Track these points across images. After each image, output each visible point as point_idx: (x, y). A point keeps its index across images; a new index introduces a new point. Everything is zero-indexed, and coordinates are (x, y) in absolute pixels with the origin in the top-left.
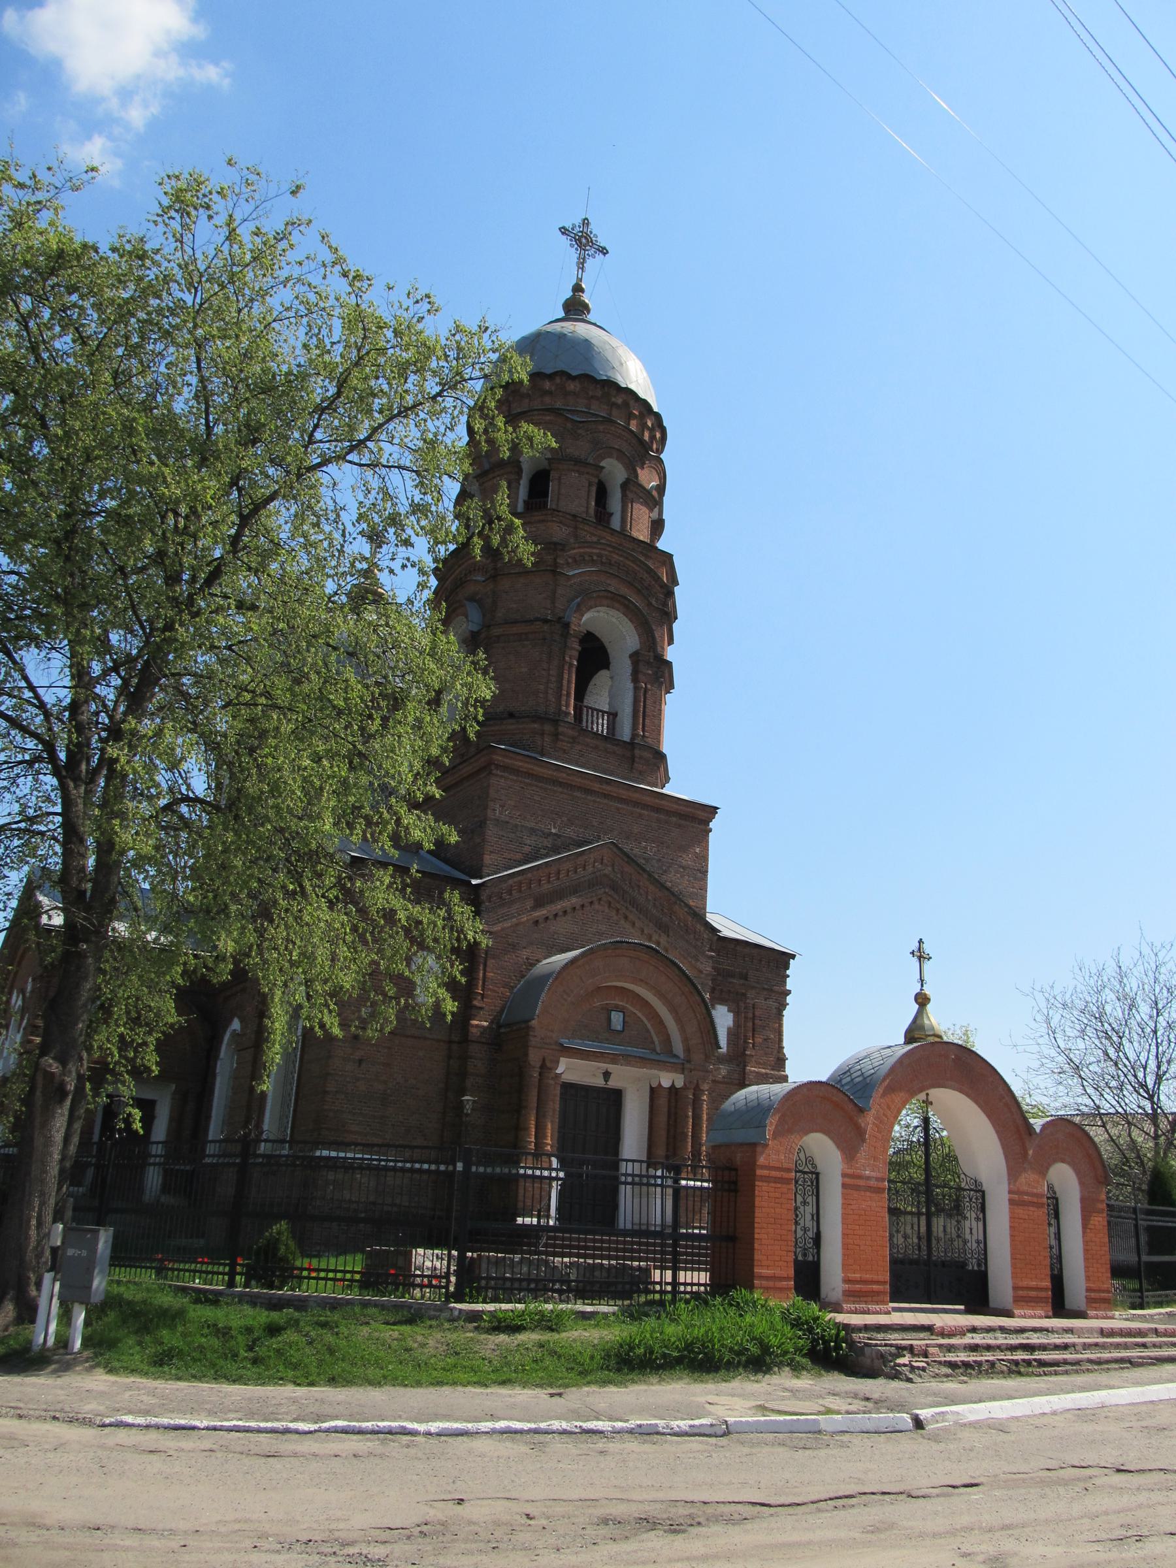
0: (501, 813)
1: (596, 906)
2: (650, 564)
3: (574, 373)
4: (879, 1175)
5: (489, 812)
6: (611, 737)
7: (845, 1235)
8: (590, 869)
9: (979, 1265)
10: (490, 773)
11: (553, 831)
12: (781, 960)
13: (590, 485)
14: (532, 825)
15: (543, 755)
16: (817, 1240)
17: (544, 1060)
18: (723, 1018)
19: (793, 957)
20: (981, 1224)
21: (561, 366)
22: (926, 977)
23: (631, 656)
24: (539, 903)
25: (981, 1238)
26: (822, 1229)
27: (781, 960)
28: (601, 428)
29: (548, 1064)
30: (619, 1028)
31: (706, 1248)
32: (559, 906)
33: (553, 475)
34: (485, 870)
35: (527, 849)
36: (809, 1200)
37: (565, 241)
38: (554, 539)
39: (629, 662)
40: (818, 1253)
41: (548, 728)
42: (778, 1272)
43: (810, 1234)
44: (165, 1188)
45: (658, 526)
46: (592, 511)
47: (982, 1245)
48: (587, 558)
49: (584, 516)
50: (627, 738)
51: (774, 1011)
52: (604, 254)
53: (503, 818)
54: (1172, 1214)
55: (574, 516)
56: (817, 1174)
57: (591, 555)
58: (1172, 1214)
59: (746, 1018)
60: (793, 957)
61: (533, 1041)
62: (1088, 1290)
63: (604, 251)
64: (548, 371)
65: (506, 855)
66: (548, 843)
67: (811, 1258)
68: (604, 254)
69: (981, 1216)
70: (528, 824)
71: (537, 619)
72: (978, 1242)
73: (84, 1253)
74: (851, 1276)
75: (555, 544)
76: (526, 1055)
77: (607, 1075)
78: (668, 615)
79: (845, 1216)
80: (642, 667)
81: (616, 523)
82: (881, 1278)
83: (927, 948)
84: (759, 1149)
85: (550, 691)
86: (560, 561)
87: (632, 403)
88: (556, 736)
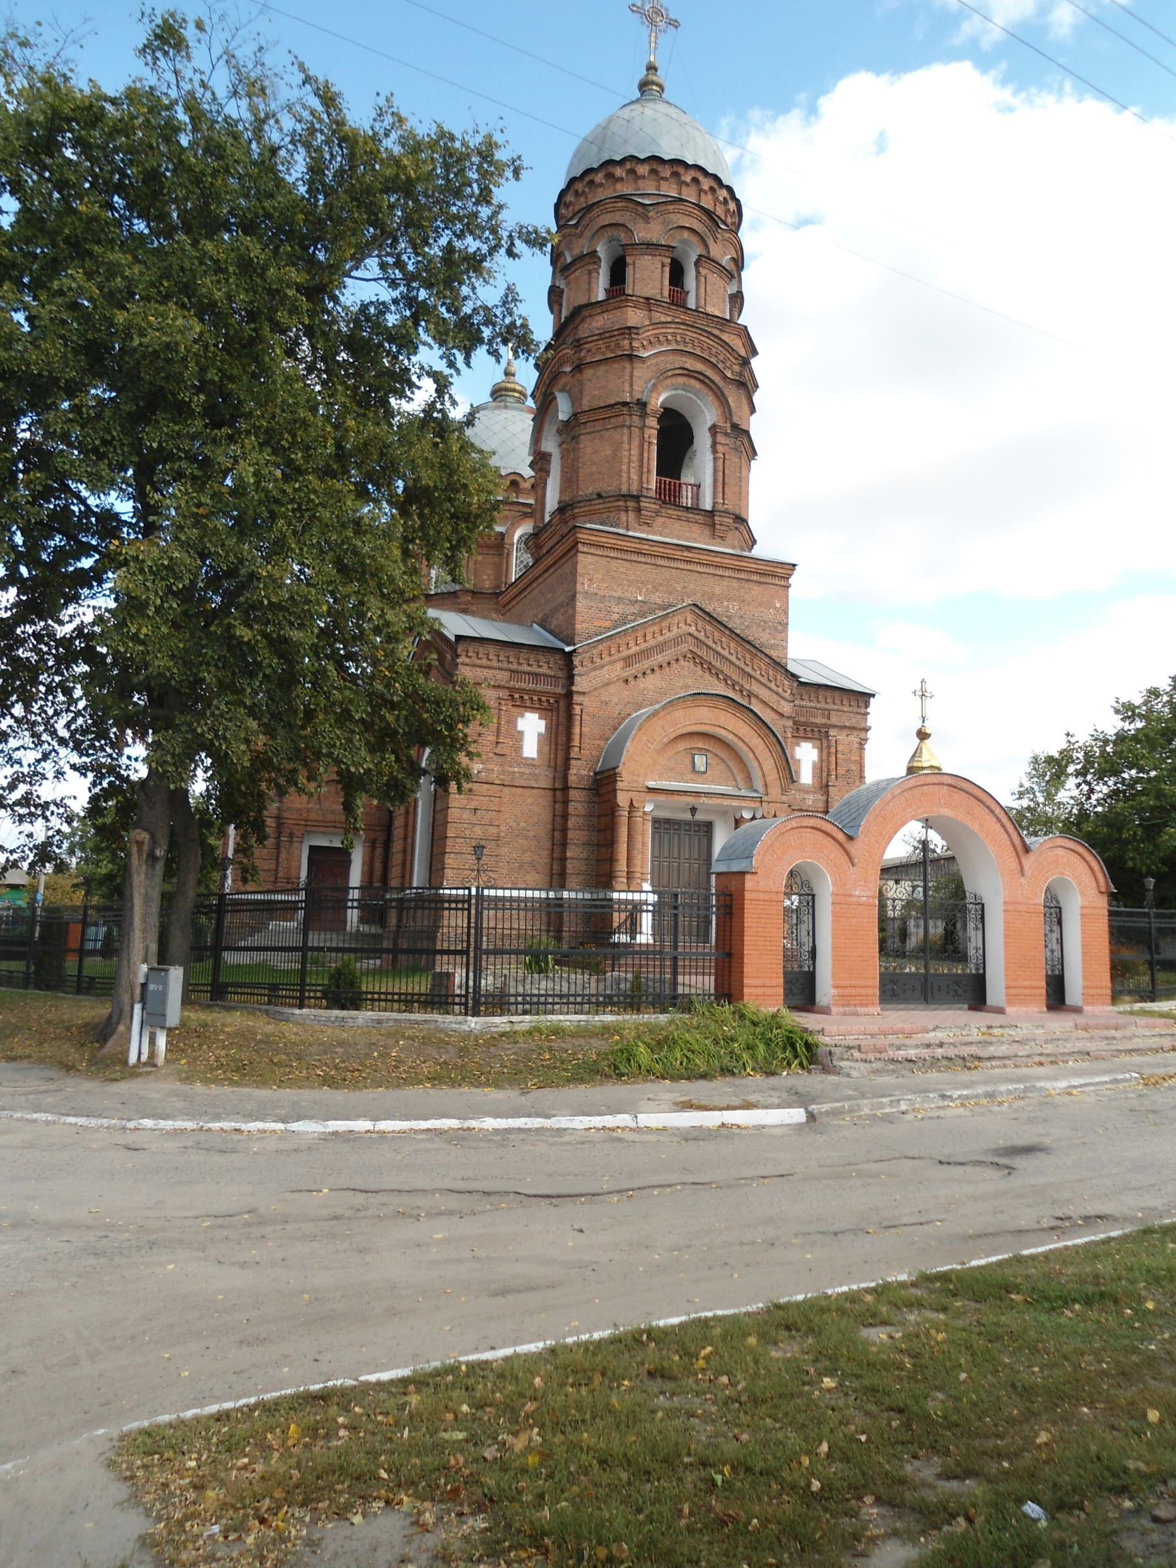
0: (589, 586)
1: (682, 662)
2: (725, 337)
3: (642, 157)
4: (868, 893)
5: (579, 586)
6: (695, 509)
7: (834, 948)
8: (675, 631)
9: (977, 969)
10: (578, 551)
11: (640, 598)
12: (863, 698)
13: (663, 265)
14: (619, 594)
15: (628, 530)
16: (813, 953)
17: (631, 803)
18: (806, 755)
19: (873, 696)
20: (980, 933)
21: (606, 157)
22: (928, 715)
23: (710, 429)
24: (628, 661)
25: (980, 944)
26: (817, 943)
27: (863, 698)
28: (671, 207)
29: (635, 804)
30: (703, 769)
31: (309, 991)
32: (646, 664)
33: (629, 260)
34: (577, 639)
35: (615, 617)
36: (805, 918)
37: (635, 18)
38: (629, 324)
39: (708, 435)
40: (814, 963)
41: (631, 504)
42: (767, 982)
43: (806, 948)
44: (362, 920)
45: (737, 299)
46: (666, 293)
47: (981, 952)
48: (661, 338)
49: (659, 298)
50: (708, 507)
51: (856, 746)
52: (676, 27)
53: (591, 590)
54: (1172, 916)
55: (648, 299)
56: (813, 896)
57: (665, 335)
58: (1172, 916)
59: (829, 753)
60: (873, 696)
61: (619, 785)
62: (1084, 987)
63: (675, 24)
64: (618, 158)
65: (596, 624)
66: (635, 609)
67: (806, 969)
68: (676, 27)
69: (980, 926)
70: (615, 594)
71: (617, 404)
72: (977, 949)
73: (161, 988)
74: (839, 983)
75: (629, 328)
76: (615, 797)
77: (693, 810)
78: (747, 385)
79: (834, 930)
80: (720, 438)
81: (691, 304)
82: (870, 983)
83: (929, 688)
84: (748, 877)
85: (632, 470)
86: (635, 344)
87: (701, 178)
88: (638, 510)
